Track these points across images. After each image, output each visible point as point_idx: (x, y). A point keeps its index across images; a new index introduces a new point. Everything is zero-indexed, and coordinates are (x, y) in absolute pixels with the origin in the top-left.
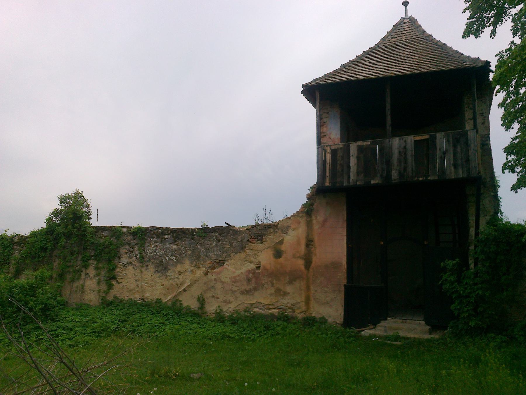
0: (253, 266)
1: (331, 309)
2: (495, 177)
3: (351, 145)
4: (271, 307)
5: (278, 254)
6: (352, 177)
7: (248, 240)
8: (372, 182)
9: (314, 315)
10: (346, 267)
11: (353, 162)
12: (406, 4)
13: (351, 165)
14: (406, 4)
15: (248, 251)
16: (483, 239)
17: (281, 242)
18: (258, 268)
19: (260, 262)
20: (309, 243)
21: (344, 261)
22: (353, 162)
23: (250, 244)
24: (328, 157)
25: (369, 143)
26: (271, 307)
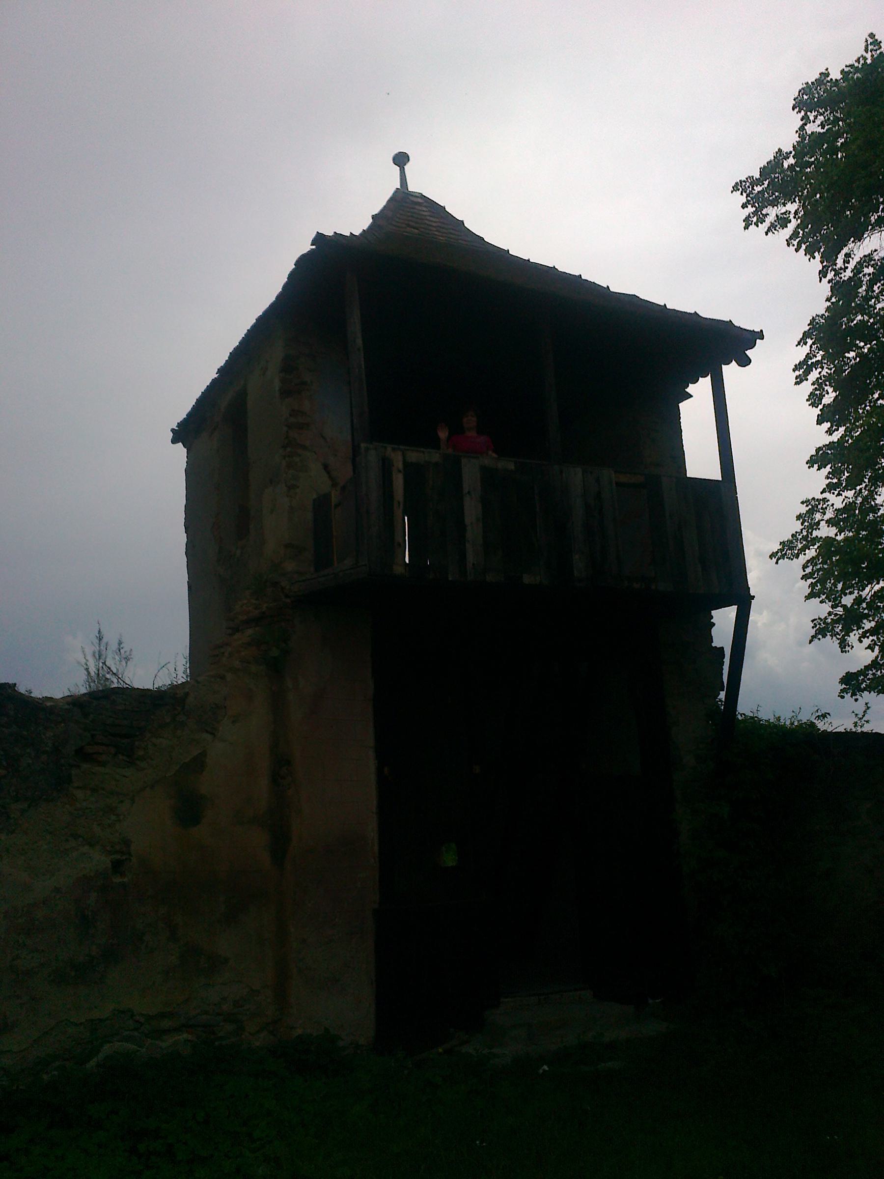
0: (98, 860)
1: (341, 1005)
2: (173, 687)
3: (464, 461)
4: (166, 1024)
5: (189, 809)
6: (471, 559)
7: (80, 751)
8: (527, 579)
9: (299, 1031)
10: (376, 848)
11: (472, 511)
12: (401, 160)
13: (468, 520)
14: (401, 160)
15: (79, 794)
16: (92, 874)
17: (198, 764)
18: (117, 866)
19: (127, 843)
20: (281, 766)
21: (371, 830)
22: (472, 511)
23: (85, 766)
24: (399, 481)
25: (512, 467)
26: (166, 1024)
